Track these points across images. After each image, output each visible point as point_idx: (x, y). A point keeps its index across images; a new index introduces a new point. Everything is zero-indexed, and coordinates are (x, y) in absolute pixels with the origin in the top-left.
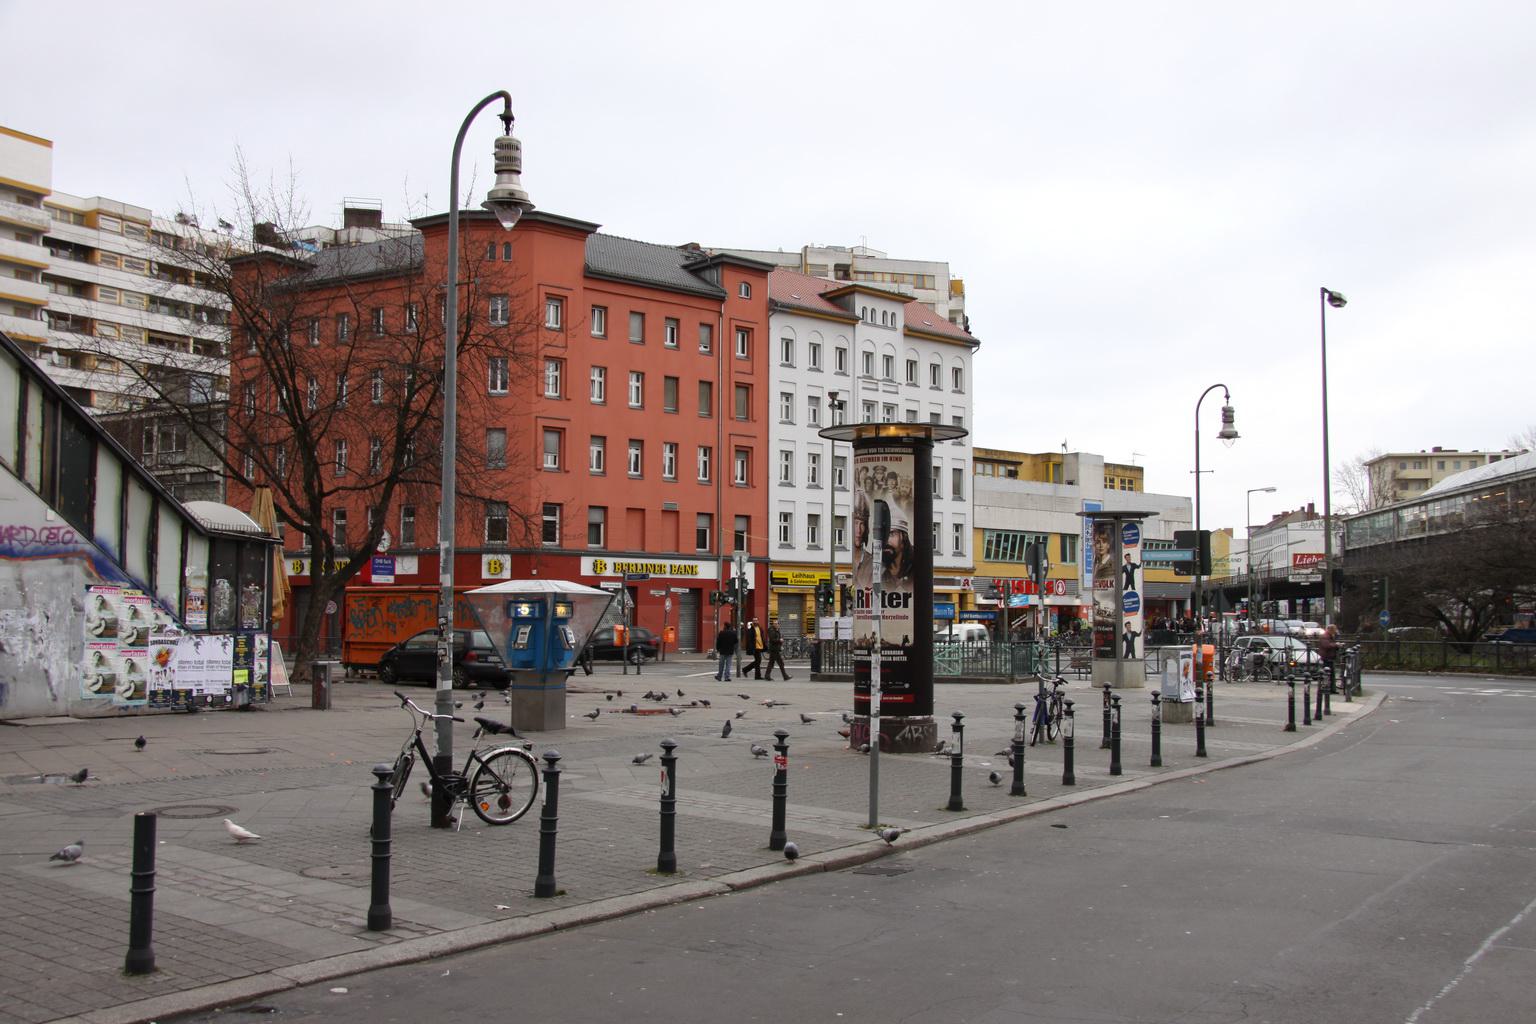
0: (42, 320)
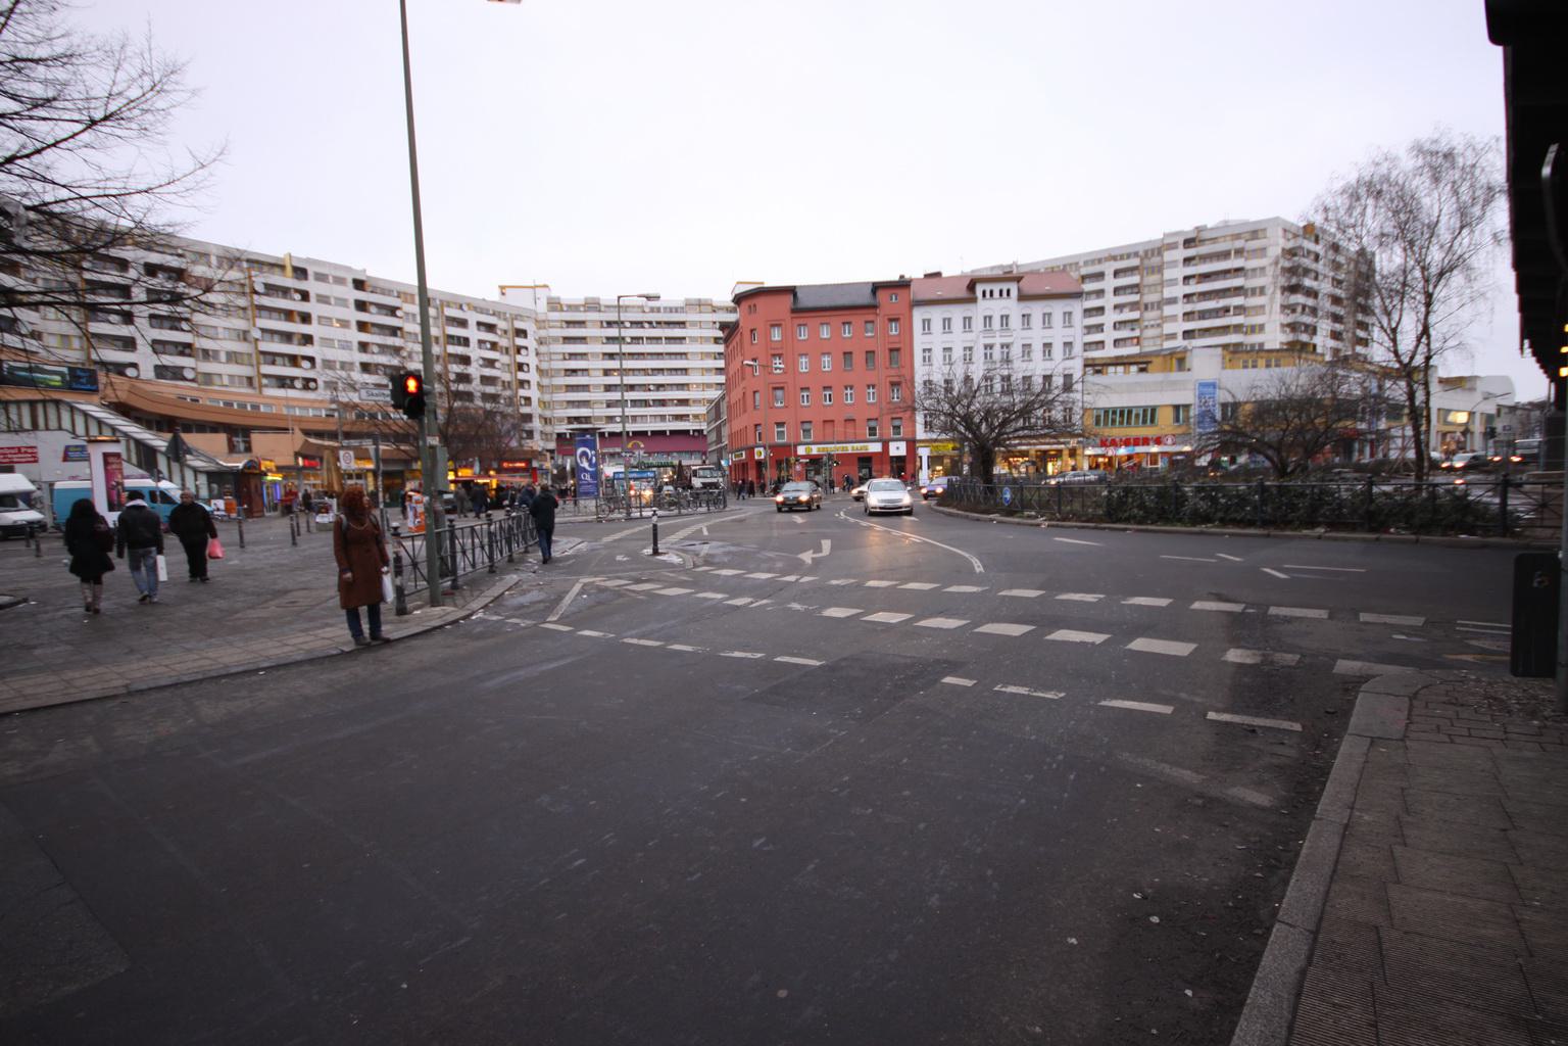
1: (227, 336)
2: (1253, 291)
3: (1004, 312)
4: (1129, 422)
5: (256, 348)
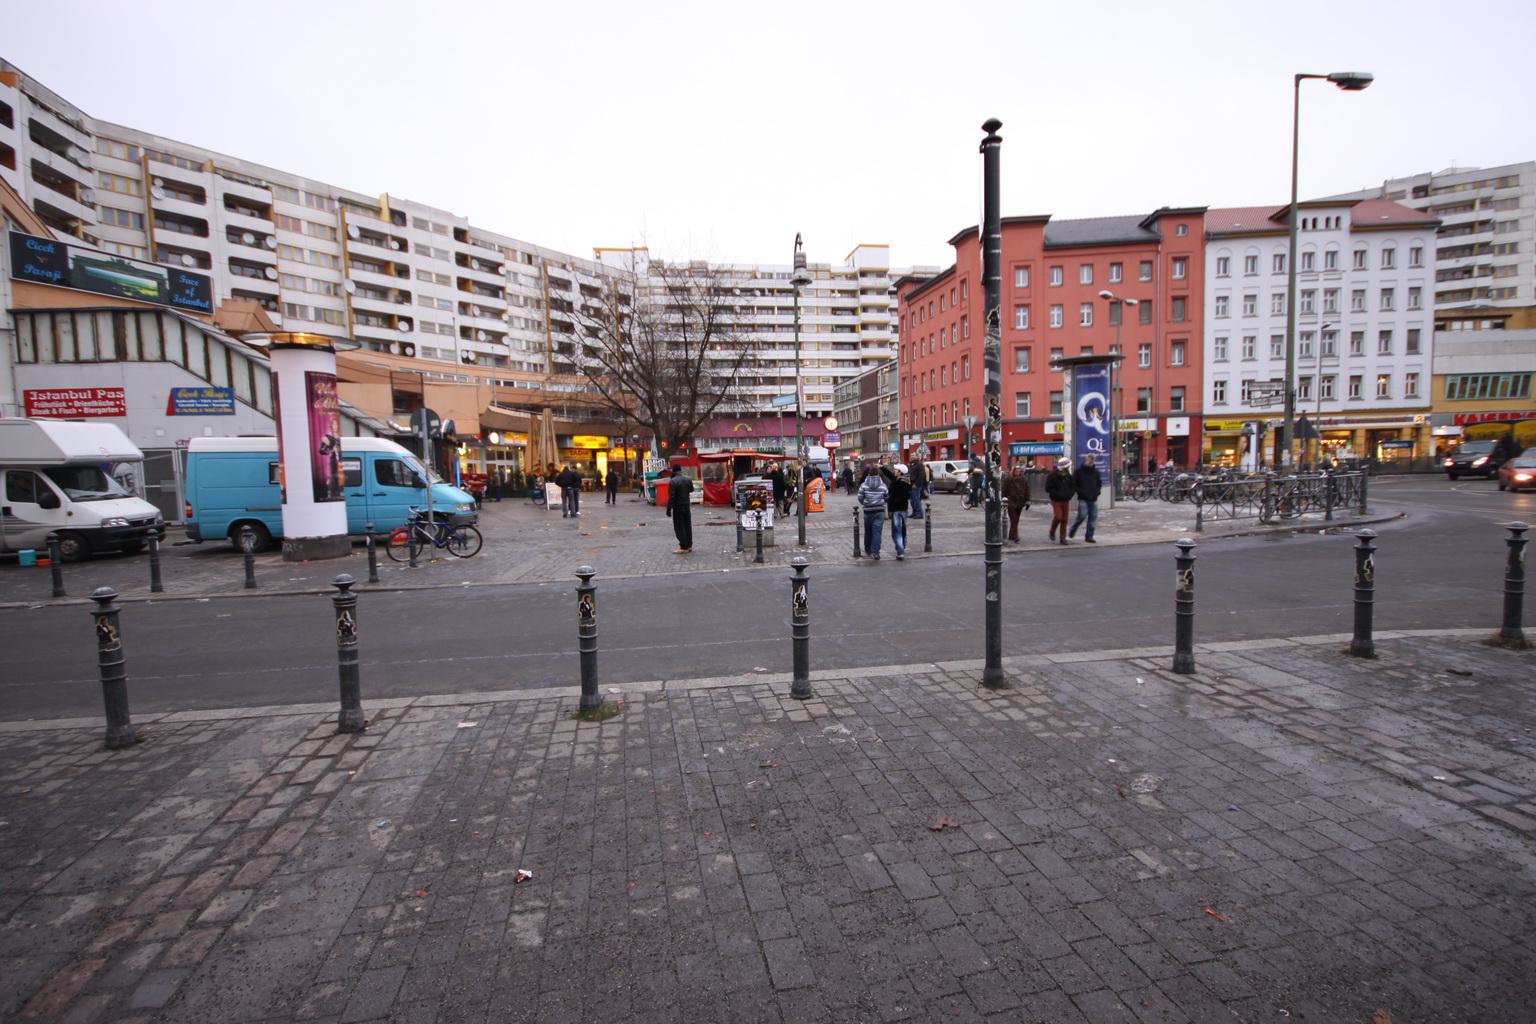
0: (163, 359)
1: (316, 289)
2: (1501, 249)
3: (1332, 248)
4: (1493, 393)
5: (349, 304)
